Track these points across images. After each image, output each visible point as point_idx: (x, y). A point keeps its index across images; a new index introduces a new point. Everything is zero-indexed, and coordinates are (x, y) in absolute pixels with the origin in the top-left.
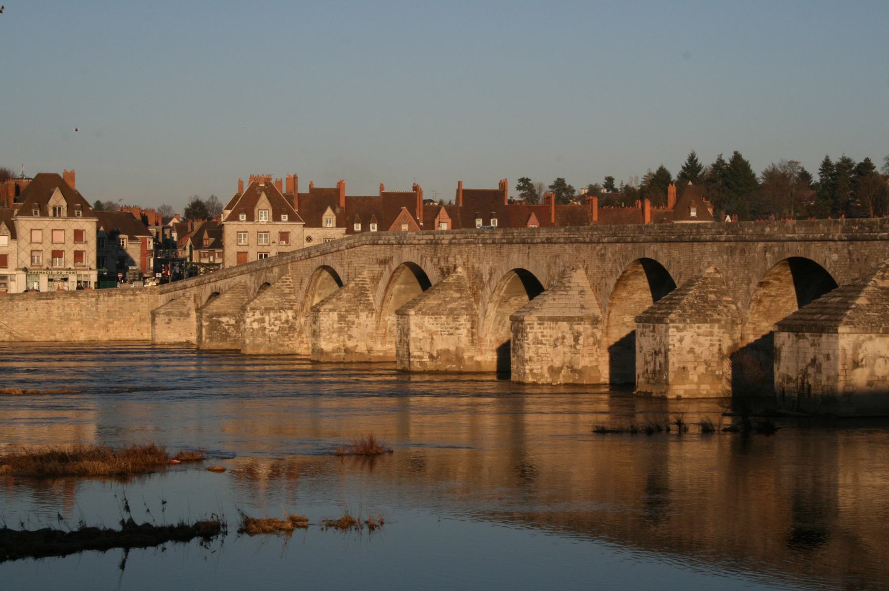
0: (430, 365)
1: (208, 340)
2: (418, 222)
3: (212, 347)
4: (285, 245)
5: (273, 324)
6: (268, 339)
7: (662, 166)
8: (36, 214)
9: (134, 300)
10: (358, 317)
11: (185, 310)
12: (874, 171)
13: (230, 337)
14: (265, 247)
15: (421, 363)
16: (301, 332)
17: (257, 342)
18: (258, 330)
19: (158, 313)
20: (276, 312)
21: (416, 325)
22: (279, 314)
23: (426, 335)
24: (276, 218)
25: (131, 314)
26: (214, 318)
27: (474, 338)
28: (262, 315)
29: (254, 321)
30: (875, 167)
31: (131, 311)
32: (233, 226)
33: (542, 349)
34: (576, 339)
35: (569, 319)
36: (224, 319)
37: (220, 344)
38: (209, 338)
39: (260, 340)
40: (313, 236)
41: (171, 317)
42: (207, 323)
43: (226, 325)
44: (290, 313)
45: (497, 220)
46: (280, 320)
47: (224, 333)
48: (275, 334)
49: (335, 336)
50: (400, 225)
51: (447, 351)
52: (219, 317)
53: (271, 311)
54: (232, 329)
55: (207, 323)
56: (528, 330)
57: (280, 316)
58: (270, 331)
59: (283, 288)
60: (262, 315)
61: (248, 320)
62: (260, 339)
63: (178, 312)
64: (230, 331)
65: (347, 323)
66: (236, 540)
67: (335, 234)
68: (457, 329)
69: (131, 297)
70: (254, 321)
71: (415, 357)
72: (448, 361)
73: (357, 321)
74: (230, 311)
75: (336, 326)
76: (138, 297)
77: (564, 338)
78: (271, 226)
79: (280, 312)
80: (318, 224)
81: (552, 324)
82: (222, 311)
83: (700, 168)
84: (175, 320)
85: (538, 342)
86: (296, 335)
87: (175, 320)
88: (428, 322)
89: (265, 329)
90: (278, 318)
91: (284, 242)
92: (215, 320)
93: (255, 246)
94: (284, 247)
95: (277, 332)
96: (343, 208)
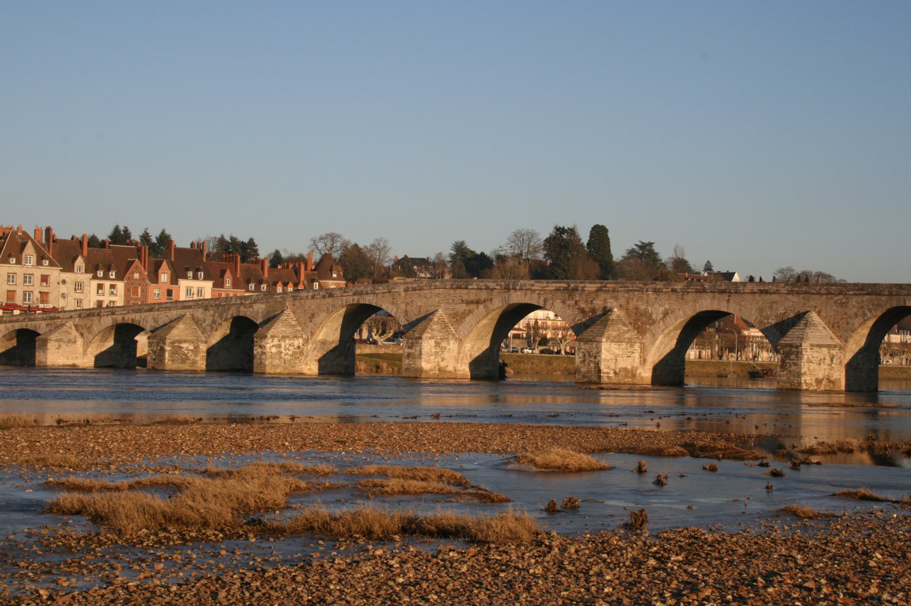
0: (615, 380)
1: (170, 362)
3: (174, 368)
5: (288, 349)
10: (449, 344)
11: (72, 337)
13: (189, 360)
15: (609, 378)
16: (306, 357)
17: (274, 363)
20: (290, 339)
21: (606, 349)
23: (612, 357)
24: (39, 263)
27: (643, 361)
29: (273, 346)
33: (813, 366)
34: (832, 360)
35: (828, 346)
38: (171, 360)
39: (277, 362)
40: (67, 280)
41: (61, 344)
44: (301, 341)
48: (289, 357)
49: (432, 358)
50: (133, 273)
51: (625, 369)
54: (190, 353)
55: (170, 348)
56: (804, 353)
59: (290, 320)
61: (268, 346)
64: (189, 355)
65: (441, 348)
66: (501, 501)
68: (633, 353)
70: (273, 346)
71: (604, 373)
72: (626, 376)
73: (448, 347)
75: (433, 350)
77: (825, 359)
81: (818, 349)
82: (184, 338)
85: (810, 361)
87: (63, 345)
88: (614, 347)
89: (281, 353)
93: (21, 286)
95: (291, 356)
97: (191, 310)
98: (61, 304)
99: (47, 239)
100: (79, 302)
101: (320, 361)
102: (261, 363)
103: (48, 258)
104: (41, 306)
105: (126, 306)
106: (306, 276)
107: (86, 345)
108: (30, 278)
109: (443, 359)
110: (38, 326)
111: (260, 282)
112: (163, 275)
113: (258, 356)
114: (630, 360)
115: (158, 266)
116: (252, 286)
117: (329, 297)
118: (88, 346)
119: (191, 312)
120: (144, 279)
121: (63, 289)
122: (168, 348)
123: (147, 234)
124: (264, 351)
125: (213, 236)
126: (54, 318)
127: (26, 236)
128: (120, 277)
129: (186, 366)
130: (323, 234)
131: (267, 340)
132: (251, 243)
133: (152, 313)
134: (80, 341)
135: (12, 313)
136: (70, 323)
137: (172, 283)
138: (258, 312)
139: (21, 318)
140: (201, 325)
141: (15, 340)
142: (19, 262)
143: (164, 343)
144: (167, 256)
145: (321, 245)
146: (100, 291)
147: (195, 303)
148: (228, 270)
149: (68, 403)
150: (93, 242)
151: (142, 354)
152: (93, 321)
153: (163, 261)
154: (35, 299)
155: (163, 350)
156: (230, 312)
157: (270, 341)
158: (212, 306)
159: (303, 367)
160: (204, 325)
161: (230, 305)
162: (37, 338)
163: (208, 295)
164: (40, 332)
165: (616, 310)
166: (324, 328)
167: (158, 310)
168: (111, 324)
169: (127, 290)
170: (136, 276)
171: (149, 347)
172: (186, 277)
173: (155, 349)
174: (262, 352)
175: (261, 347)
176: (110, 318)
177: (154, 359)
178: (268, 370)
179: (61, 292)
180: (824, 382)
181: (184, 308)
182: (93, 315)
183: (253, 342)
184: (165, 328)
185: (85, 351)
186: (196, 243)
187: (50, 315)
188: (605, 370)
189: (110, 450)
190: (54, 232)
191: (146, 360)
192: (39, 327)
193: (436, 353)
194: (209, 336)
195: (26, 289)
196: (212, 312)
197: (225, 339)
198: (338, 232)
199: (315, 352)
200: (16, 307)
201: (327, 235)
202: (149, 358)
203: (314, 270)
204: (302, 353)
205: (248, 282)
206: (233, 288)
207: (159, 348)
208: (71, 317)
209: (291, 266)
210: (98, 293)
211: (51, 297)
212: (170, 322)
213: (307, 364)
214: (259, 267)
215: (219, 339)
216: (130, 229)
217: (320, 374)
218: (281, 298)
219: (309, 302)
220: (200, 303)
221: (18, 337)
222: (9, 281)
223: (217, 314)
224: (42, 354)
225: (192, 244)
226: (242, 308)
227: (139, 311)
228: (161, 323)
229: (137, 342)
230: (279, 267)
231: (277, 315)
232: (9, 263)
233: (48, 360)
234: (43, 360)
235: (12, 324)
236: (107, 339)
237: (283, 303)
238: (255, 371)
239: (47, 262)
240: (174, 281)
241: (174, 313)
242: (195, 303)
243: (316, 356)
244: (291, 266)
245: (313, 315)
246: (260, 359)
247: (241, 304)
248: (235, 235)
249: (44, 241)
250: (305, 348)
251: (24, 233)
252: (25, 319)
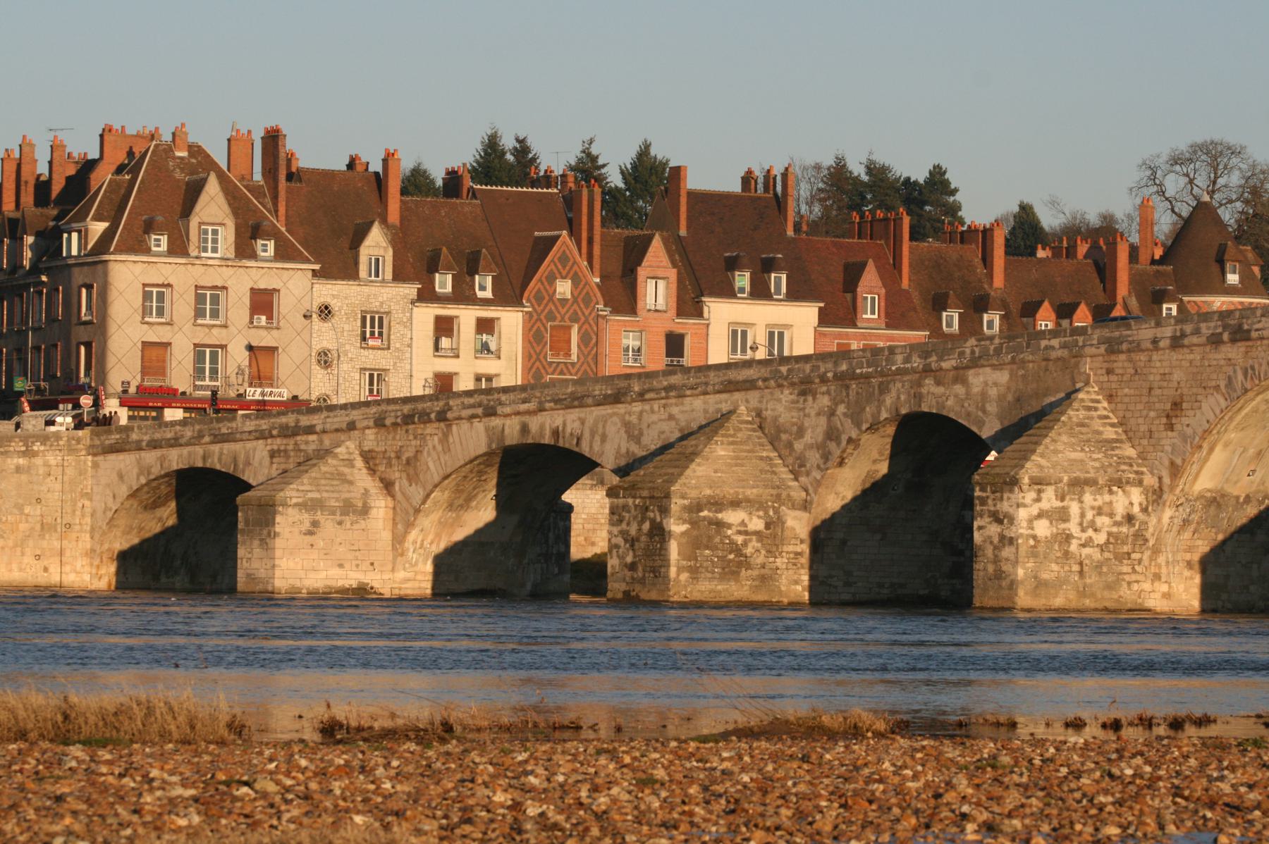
1: (684, 576)
3: (696, 596)
4: (266, 328)
6: (1076, 568)
7: (419, 164)
8: (805, 169)
9: (28, 470)
11: (355, 495)
12: (952, 199)
13: (749, 567)
14: (215, 331)
16: (1156, 551)
18: (1050, 541)
19: (285, 505)
20: (1099, 491)
22: (1107, 498)
24: (244, 250)
25: (20, 508)
26: (705, 513)
28: (1062, 500)
29: (1040, 516)
30: (956, 191)
31: (21, 501)
32: (131, 265)
36: (733, 517)
37: (719, 587)
39: (1051, 571)
40: (335, 304)
41: (319, 516)
42: (684, 527)
43: (739, 532)
44: (1136, 496)
45: (784, 277)
46: (1111, 515)
47: (732, 556)
48: (1096, 554)
50: (551, 279)
52: (720, 511)
53: (1086, 488)
54: (754, 544)
55: (684, 527)
57: (1111, 503)
58: (1084, 546)
59: (1097, 424)
60: (1062, 500)
61: (1022, 514)
62: (1054, 567)
63: (337, 500)
64: (749, 551)
67: (390, 300)
69: (21, 461)
70: (1040, 516)
74: (751, 493)
76: (38, 461)
78: (230, 271)
79: (1111, 492)
82: (729, 491)
84: (328, 525)
86: (1147, 554)
87: (328, 525)
89: (1068, 538)
90: (1106, 509)
91: (264, 318)
92: (704, 518)
93: (188, 327)
94: (263, 333)
95: (1102, 548)
96: (394, 227)
97: (753, 396)
98: (318, 385)
99: (270, 170)
100: (375, 377)
101: (1208, 564)
102: (999, 575)
103: (275, 235)
104: (254, 394)
105: (533, 387)
106: (1137, 282)
107: (404, 520)
108: (215, 300)
110: (242, 458)
111: (979, 304)
112: (651, 283)
113: (989, 551)
115: (634, 254)
116: (952, 319)
117: (1233, 341)
118: (409, 525)
119: (754, 403)
120: (587, 301)
121: (323, 336)
122: (676, 527)
123: (593, 159)
124: (1009, 533)
125: (810, 161)
126: (294, 431)
127: (201, 160)
128: (508, 295)
129: (740, 589)
130: (1182, 145)
131: (1017, 496)
132: (938, 182)
133: (621, 408)
134: (381, 507)
135: (160, 417)
136: (348, 448)
137: (680, 313)
138: (984, 395)
139: (188, 433)
140: (790, 445)
141: (173, 505)
142: (179, 248)
143: (665, 511)
144: (665, 223)
145: (1174, 184)
146: (445, 342)
147: (764, 372)
148: (871, 264)
149: (353, 678)
150: (417, 182)
151: (588, 553)
152: (423, 437)
153: (654, 235)
154: (232, 370)
155: (659, 533)
156: (889, 400)
158: (824, 380)
159: (1147, 586)
160: (798, 446)
161: (887, 379)
162: (239, 499)
163: (802, 341)
164: (248, 477)
166: (1218, 449)
167: (641, 396)
168: (483, 449)
169: (533, 337)
170: (564, 288)
171: (612, 523)
172: (728, 292)
173: (633, 530)
174: (1002, 537)
175: (997, 518)
176: (479, 426)
177: (632, 567)
178: (1023, 599)
179: (317, 346)
181: (731, 387)
182: (425, 418)
183: (968, 503)
184: (666, 457)
185: (398, 540)
186: (759, 173)
187: (284, 420)
189: (599, 816)
190: (291, 144)
191: (604, 565)
192: (248, 463)
194: (818, 483)
195: (202, 337)
196: (825, 401)
197: (872, 494)
198: (1232, 139)
199: (1187, 535)
200: (171, 396)
201: (1197, 148)
202: (613, 563)
203: (1163, 260)
204: (1140, 537)
205: (939, 304)
206: (889, 326)
207: (646, 526)
208: (351, 426)
209: (1083, 249)
210: (437, 348)
211: (285, 365)
212: (684, 438)
213: (1157, 577)
214: (973, 253)
215: (849, 495)
216: (536, 146)
217: (1203, 611)
218: (1064, 346)
219: (1163, 361)
220: (784, 369)
221: (179, 495)
222: (146, 311)
223: (841, 409)
224: (257, 551)
225: (748, 179)
226: (929, 385)
227: (577, 401)
228: (651, 441)
229: (570, 508)
230: (1041, 254)
231: (1053, 405)
232: (148, 251)
233: (278, 573)
234: (262, 574)
235: (158, 453)
236: (469, 499)
237: (1070, 364)
238: (977, 602)
239: (271, 245)
240: (690, 305)
241: (696, 408)
242: (764, 372)
243: (1190, 549)
244: (1083, 249)
245: (1177, 405)
246: (996, 560)
247: (927, 370)
248: (881, 158)
249: (258, 176)
250: (1153, 521)
251: (195, 150)
252: (200, 436)
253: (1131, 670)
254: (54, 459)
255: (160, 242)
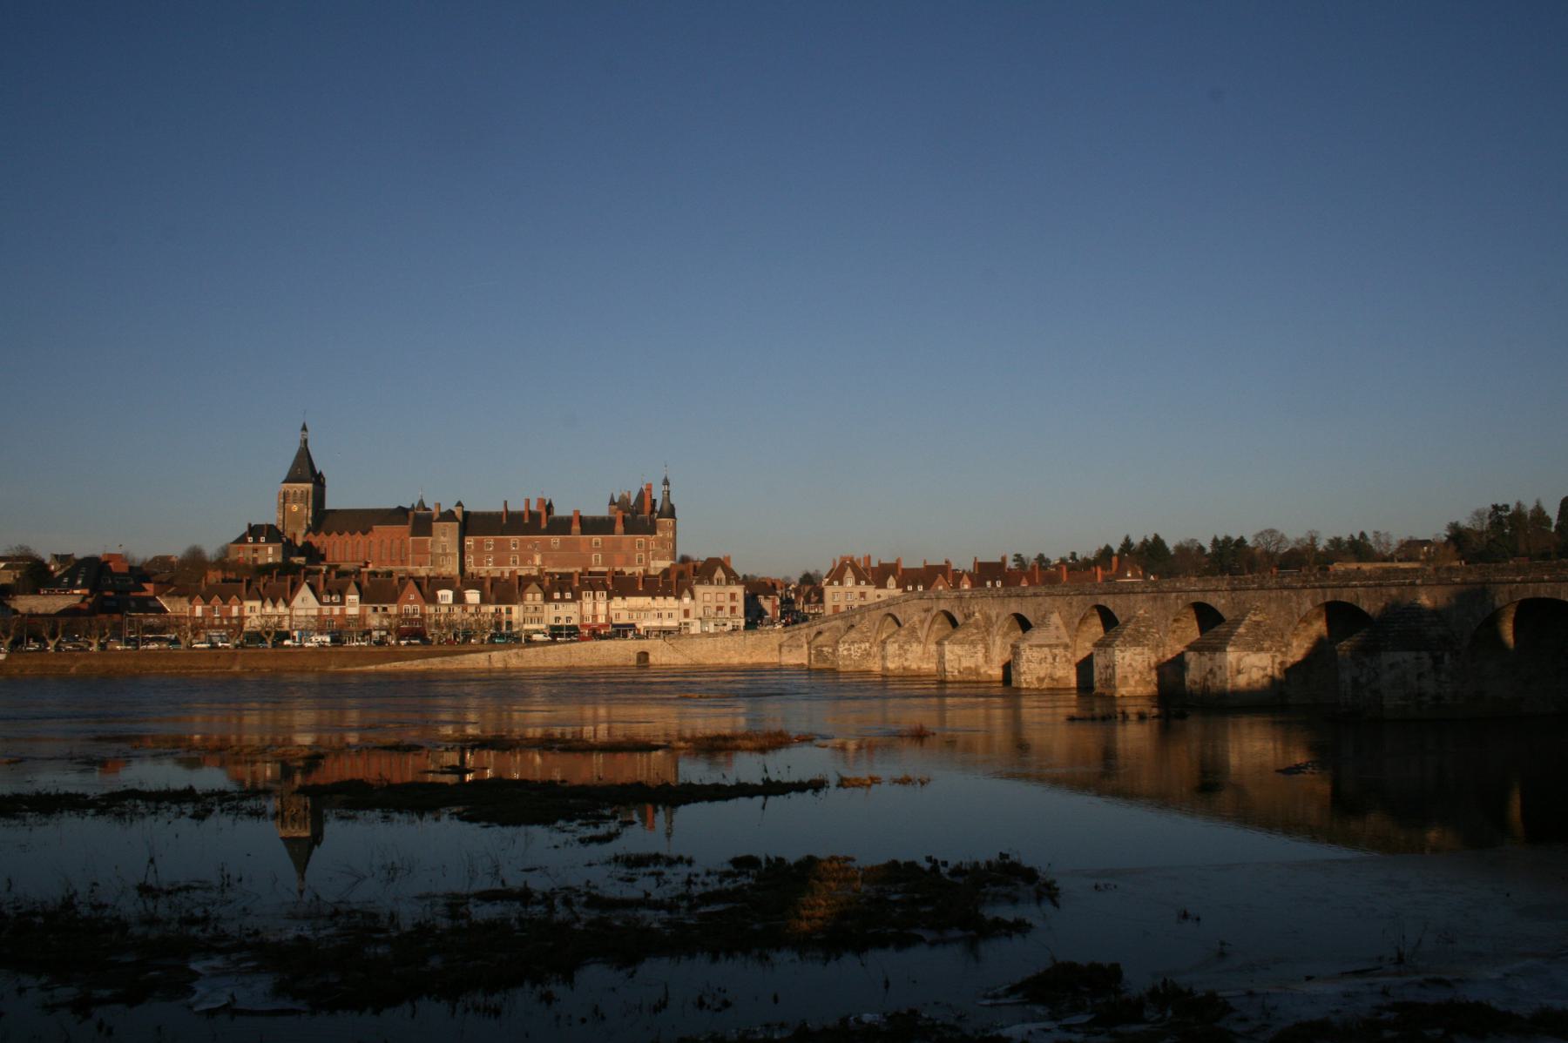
2: (949, 584)
9: (768, 637)
23: (956, 657)
34: (1054, 659)
35: (1050, 646)
36: (825, 649)
39: (847, 662)
44: (867, 645)
49: (897, 659)
51: (969, 668)
61: (840, 650)
68: (976, 653)
72: (970, 674)
75: (897, 652)
77: (1046, 658)
80: (884, 586)
81: (1038, 650)
82: (824, 643)
83: (1132, 545)
85: (1029, 661)
109: (906, 660)
114: (973, 660)
157: (842, 645)
165: (977, 614)
170: (940, 588)
180: (1046, 681)
188: (950, 670)
193: (900, 655)
253: (260, 753)
254: (774, 635)
255: (836, 583)
